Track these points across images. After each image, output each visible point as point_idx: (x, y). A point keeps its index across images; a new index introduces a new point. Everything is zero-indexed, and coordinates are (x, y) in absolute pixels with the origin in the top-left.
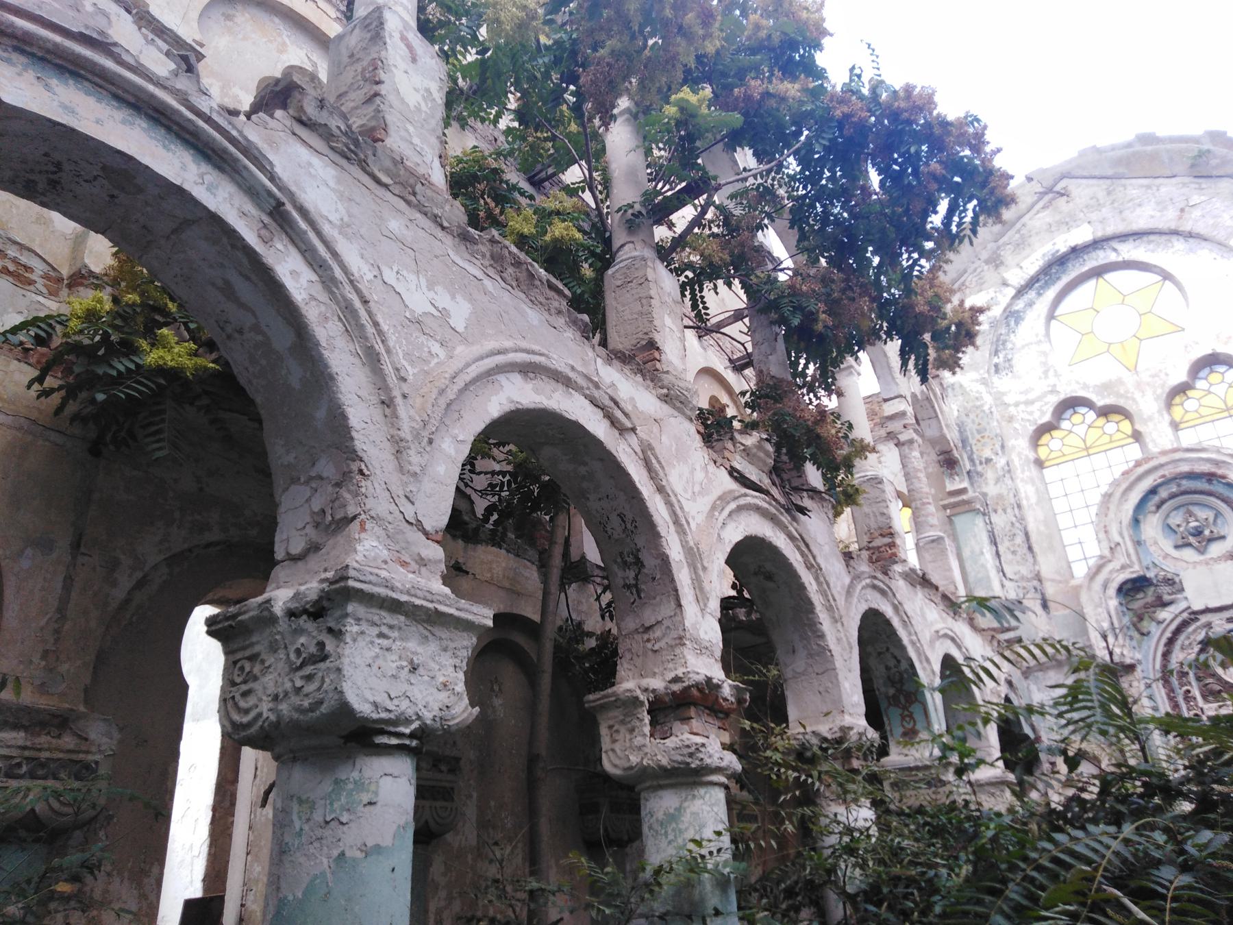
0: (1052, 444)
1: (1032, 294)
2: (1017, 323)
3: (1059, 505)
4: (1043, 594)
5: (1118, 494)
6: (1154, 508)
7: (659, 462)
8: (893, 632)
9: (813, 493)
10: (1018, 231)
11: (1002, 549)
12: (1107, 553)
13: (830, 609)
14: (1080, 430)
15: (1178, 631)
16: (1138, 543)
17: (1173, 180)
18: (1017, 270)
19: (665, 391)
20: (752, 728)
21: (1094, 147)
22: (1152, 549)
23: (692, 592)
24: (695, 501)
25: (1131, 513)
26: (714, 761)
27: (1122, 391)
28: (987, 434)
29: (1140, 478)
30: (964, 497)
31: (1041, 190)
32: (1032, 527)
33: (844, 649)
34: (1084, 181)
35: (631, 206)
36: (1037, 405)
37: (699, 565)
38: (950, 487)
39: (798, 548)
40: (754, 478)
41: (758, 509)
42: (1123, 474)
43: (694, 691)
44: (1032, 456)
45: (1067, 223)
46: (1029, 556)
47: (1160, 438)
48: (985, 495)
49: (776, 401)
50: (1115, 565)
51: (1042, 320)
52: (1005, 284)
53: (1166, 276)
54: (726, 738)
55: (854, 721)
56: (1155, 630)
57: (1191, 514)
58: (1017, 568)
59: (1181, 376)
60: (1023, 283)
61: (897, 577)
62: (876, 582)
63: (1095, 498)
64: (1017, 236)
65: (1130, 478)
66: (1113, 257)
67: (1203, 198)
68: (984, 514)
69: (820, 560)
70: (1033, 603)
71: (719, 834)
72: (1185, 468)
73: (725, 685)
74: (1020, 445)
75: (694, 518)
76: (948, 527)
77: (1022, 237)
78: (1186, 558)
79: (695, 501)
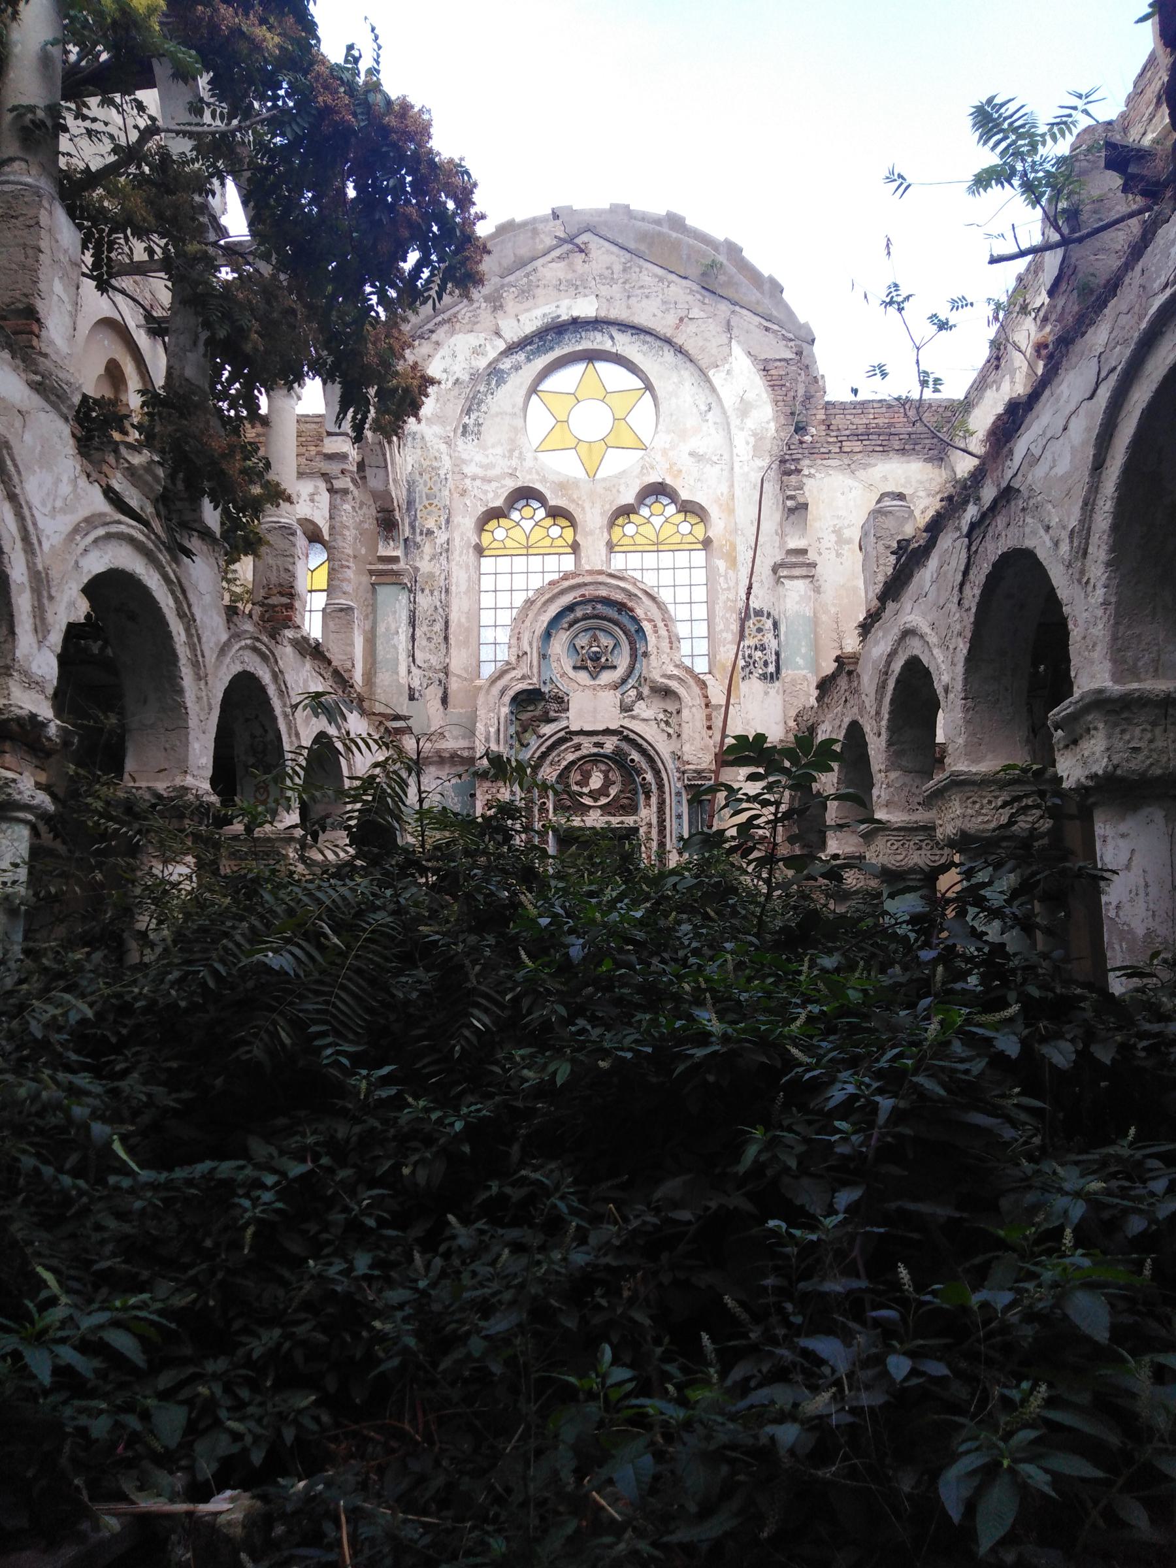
0: (498, 531)
1: (521, 357)
2: (498, 385)
3: (487, 600)
4: (446, 689)
5: (539, 604)
6: (566, 626)
7: (16, 466)
8: (267, 700)
9: (206, 534)
10: (527, 275)
11: (418, 633)
12: (513, 660)
13: (195, 664)
14: (527, 525)
15: (551, 748)
16: (544, 656)
17: (684, 281)
19: (38, 378)
20: (77, 774)
21: (627, 207)
22: (554, 665)
23: (31, 621)
24: (53, 518)
25: (545, 625)
26: (25, 798)
27: (575, 497)
28: (435, 502)
29: (563, 592)
30: (395, 567)
31: (562, 235)
32: (454, 617)
33: (202, 709)
34: (607, 244)
35: (32, 109)
36: (494, 484)
37: (45, 594)
38: (383, 551)
39: (173, 593)
40: (134, 503)
41: (131, 540)
42: (549, 584)
43: (14, 726)
44: (474, 540)
45: (576, 287)
46: (443, 646)
47: (594, 557)
48: (416, 569)
49: (182, 416)
50: (517, 673)
51: (523, 392)
52: (498, 334)
53: (649, 387)
54: (43, 778)
55: (197, 783)
56: (534, 742)
57: (595, 638)
58: (428, 656)
59: (629, 498)
60: (516, 340)
61: (286, 643)
62: (258, 644)
63: (519, 599)
64: (525, 279)
65: (554, 590)
66: (608, 345)
67: (702, 315)
68: (410, 591)
69: (197, 611)
70: (434, 693)
71: (16, 865)
72: (603, 592)
73: (52, 724)
74: (465, 523)
75: (48, 537)
76: (369, 595)
78: (579, 681)
79: (53, 518)
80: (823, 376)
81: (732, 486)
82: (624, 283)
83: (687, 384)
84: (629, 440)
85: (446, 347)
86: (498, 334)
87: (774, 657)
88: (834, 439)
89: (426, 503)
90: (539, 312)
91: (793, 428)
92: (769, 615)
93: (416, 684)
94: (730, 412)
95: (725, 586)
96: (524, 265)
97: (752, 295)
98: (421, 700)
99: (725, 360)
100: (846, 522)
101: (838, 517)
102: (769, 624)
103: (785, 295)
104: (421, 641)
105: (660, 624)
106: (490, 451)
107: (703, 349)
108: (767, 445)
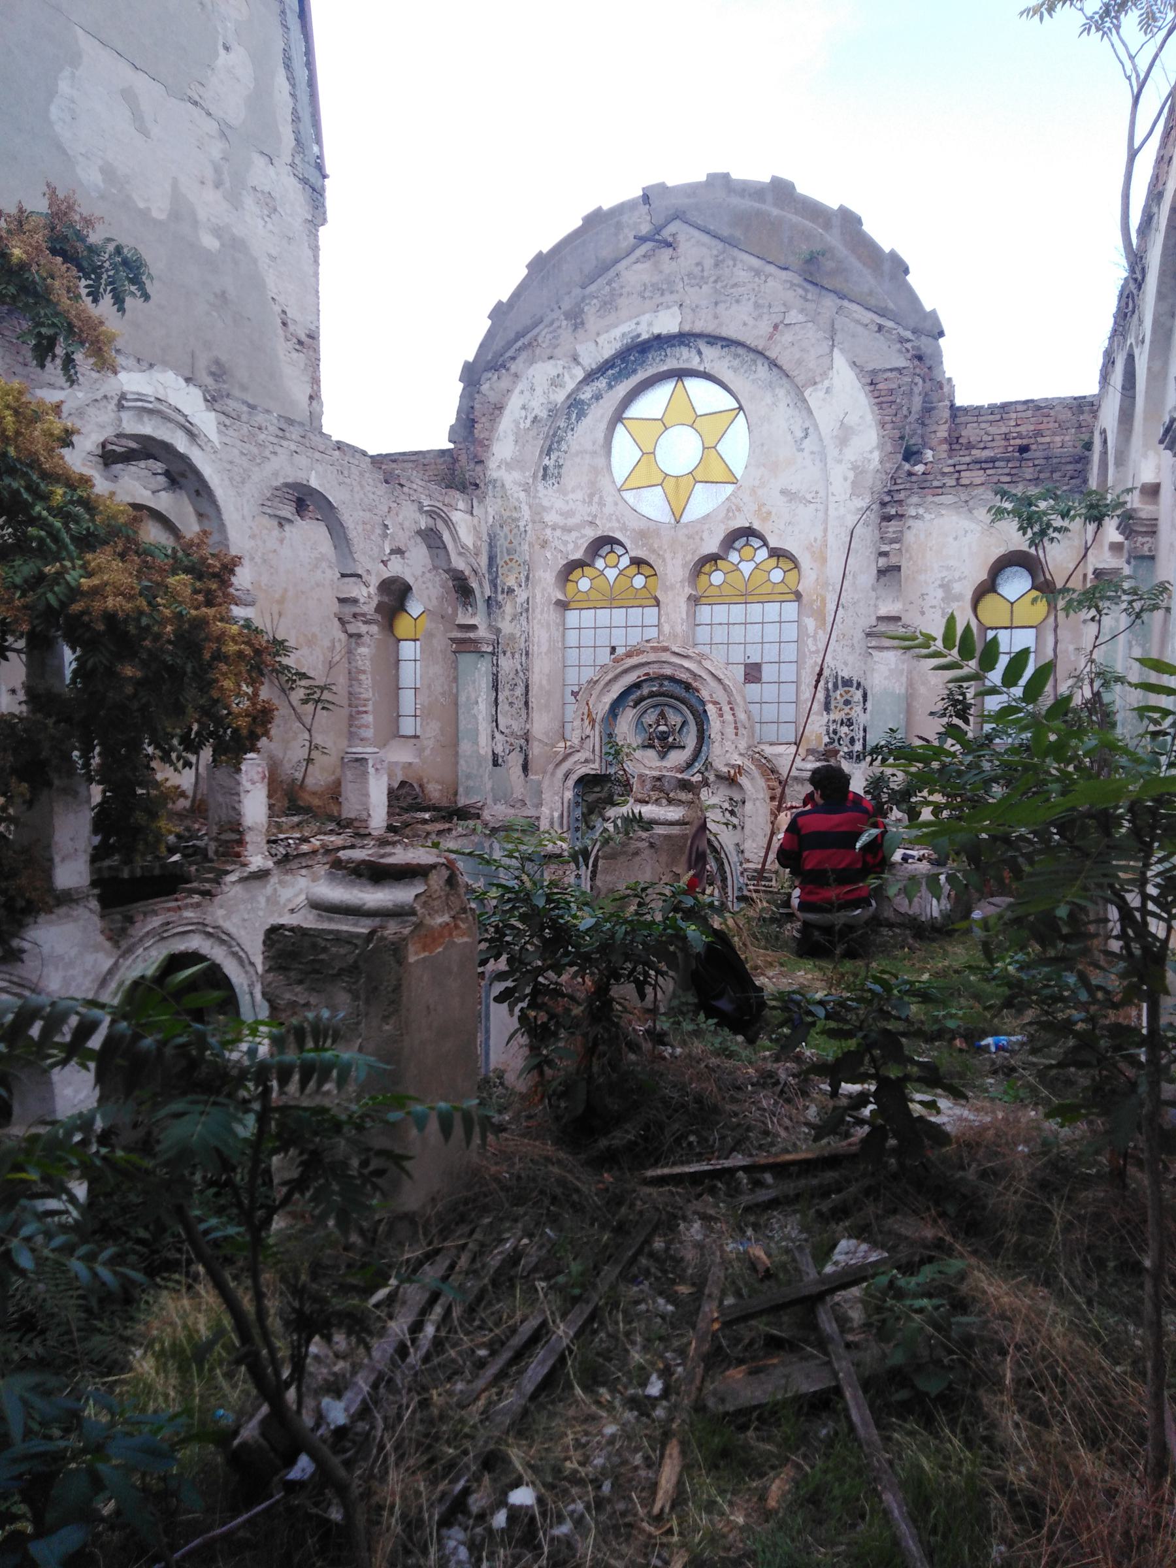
1: (602, 383)
2: (578, 419)
4: (526, 756)
5: (603, 683)
11: (501, 698)
17: (784, 273)
18: (591, 346)
21: (726, 176)
25: (607, 707)
28: (516, 557)
30: (472, 635)
34: (696, 233)
36: (574, 534)
46: (524, 712)
51: (603, 425)
57: (662, 715)
59: (712, 546)
60: (594, 366)
64: (607, 288)
66: (695, 363)
70: (516, 760)
72: (668, 671)
74: (546, 577)
77: (612, 293)
80: (950, 380)
81: (825, 530)
82: (715, 282)
83: (782, 405)
84: (718, 473)
85: (524, 379)
86: (575, 359)
87: (862, 734)
88: (951, 469)
89: (507, 558)
90: (617, 332)
91: (900, 457)
92: (859, 684)
93: (499, 750)
94: (827, 441)
95: (813, 649)
96: (608, 269)
97: (864, 280)
98: (505, 766)
99: (824, 374)
100: (957, 575)
101: (948, 568)
102: (858, 695)
103: (910, 278)
104: (503, 707)
105: (726, 708)
106: (571, 496)
107: (799, 362)
108: (869, 480)
